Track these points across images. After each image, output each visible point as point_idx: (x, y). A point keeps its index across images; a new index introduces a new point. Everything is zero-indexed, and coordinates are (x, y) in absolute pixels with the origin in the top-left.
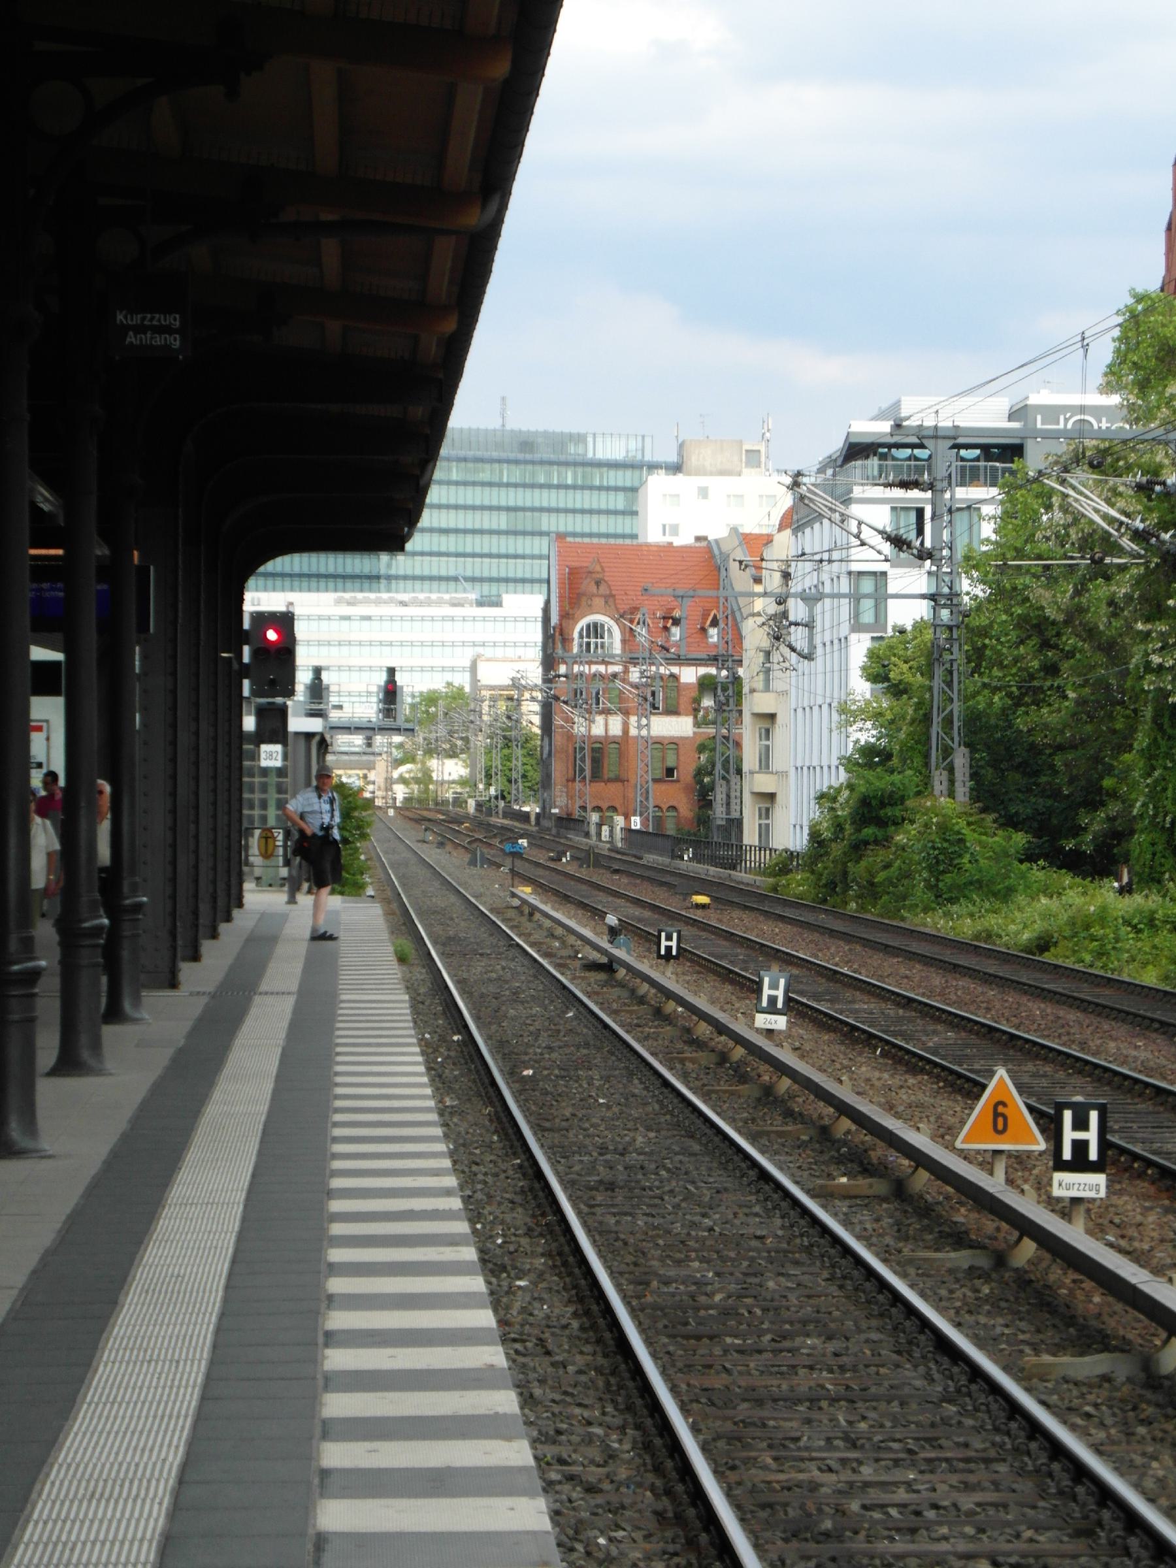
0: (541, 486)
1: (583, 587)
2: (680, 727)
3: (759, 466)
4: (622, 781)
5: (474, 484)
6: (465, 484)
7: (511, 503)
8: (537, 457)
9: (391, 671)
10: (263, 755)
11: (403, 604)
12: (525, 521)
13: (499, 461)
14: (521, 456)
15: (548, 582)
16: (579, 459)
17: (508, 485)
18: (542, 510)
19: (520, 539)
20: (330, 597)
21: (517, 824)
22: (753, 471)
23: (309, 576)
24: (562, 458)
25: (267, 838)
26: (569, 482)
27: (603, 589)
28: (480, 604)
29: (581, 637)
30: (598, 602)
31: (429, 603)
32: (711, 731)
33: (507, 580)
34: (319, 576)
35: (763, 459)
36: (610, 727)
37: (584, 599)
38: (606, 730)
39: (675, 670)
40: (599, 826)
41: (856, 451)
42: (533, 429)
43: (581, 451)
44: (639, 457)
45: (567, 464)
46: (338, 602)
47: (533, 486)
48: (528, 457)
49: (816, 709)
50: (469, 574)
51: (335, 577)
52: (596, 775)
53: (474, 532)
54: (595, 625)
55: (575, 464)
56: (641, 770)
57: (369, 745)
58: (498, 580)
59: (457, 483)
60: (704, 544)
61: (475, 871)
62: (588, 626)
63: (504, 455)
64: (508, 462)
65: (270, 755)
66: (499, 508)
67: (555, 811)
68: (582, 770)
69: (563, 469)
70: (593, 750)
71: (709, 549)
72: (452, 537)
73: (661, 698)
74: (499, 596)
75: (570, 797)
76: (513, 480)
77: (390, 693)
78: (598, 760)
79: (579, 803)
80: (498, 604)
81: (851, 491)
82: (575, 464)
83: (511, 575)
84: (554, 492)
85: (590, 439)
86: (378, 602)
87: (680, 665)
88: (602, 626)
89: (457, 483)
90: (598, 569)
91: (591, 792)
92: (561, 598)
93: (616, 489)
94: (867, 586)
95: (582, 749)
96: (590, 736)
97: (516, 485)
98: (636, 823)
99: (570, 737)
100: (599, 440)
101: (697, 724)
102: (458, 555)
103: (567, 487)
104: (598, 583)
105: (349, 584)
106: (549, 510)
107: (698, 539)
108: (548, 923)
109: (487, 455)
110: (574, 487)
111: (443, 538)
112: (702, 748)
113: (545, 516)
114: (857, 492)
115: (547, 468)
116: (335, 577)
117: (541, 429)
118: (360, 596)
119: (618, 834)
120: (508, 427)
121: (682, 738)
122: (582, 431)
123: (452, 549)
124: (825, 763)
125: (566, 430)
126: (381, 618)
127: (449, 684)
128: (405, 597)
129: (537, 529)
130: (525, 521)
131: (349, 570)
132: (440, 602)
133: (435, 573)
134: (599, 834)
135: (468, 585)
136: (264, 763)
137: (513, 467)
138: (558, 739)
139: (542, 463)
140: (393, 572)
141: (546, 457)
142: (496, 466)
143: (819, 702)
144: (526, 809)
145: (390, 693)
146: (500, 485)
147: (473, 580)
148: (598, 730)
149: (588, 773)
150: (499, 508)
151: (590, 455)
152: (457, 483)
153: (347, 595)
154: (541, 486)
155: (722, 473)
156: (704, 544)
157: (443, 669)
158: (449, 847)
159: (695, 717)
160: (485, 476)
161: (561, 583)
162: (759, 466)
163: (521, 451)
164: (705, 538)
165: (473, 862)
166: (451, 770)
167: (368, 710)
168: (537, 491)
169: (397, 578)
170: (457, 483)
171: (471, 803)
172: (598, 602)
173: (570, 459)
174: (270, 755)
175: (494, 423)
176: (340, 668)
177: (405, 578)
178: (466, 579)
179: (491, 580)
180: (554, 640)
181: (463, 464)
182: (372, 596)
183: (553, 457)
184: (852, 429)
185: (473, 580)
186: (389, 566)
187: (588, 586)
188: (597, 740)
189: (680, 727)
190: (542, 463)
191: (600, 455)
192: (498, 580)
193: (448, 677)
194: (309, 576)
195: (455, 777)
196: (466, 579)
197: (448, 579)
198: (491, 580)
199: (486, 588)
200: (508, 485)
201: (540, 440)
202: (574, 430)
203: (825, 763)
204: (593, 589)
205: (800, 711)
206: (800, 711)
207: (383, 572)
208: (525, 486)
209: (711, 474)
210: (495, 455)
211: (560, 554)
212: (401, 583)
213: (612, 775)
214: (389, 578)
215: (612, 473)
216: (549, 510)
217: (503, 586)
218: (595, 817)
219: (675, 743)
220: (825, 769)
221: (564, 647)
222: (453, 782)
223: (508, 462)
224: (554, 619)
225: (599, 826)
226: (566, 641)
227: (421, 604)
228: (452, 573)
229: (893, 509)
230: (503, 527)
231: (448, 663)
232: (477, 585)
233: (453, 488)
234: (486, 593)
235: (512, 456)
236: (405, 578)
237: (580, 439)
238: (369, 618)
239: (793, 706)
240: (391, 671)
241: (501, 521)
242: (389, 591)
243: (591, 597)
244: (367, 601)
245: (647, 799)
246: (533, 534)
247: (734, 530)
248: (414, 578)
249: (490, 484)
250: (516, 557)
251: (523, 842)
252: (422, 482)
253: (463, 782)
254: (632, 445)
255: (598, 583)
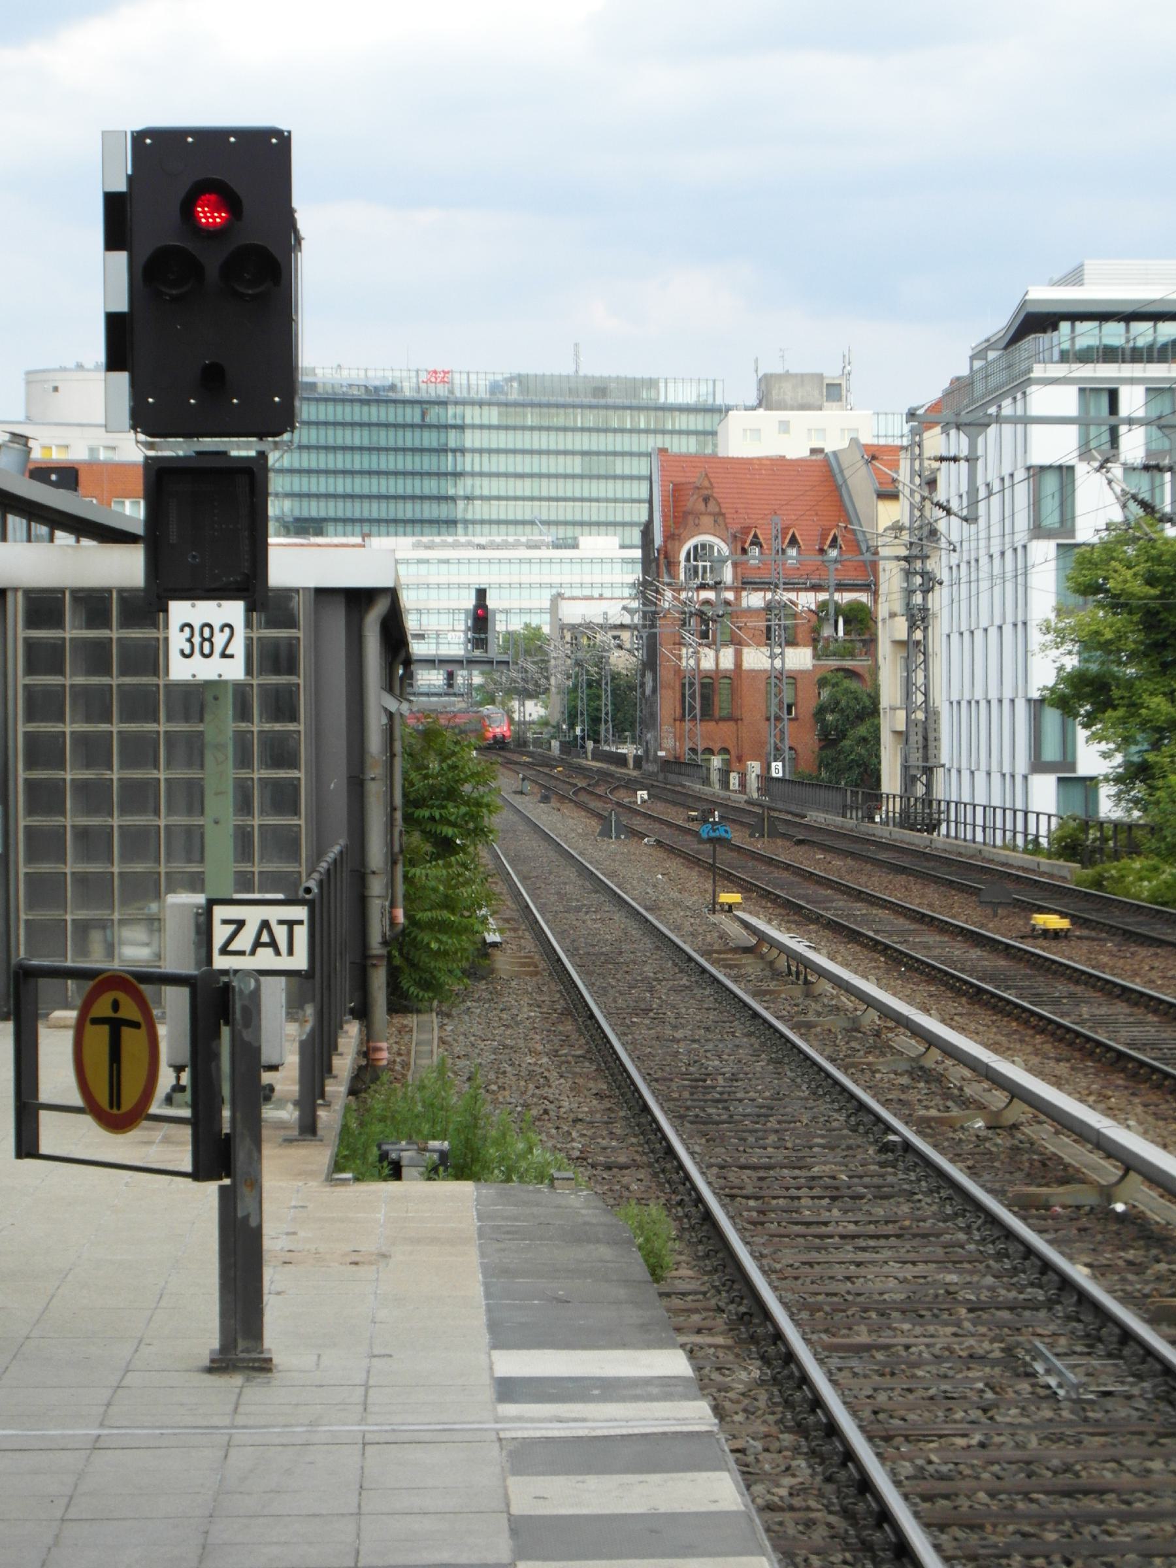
0: (615, 431)
1: (690, 504)
2: (800, 658)
3: (840, 400)
4: (736, 720)
5: (549, 429)
6: (540, 428)
7: (586, 448)
8: (610, 401)
9: (481, 594)
10: (177, 641)
11: (481, 547)
12: (599, 465)
13: (574, 406)
14: (594, 401)
15: (650, 502)
16: (652, 404)
17: (583, 430)
18: (615, 454)
19: (594, 483)
20: (409, 540)
21: (613, 768)
22: (835, 404)
23: (387, 521)
24: (635, 402)
25: (116, 1026)
26: (642, 426)
27: (712, 506)
28: (556, 546)
29: (688, 559)
30: (707, 521)
31: (504, 546)
32: (833, 663)
33: (582, 524)
34: (396, 521)
35: (844, 393)
36: (721, 660)
37: (691, 518)
38: (717, 665)
39: (792, 596)
40: (725, 773)
41: (1036, 322)
42: (606, 374)
43: (653, 394)
44: (710, 401)
45: (640, 408)
46: (416, 546)
47: (606, 430)
48: (602, 402)
49: (979, 634)
50: (544, 517)
51: (413, 522)
52: (707, 713)
53: (558, 453)
54: (703, 546)
55: (647, 408)
56: (754, 705)
57: (450, 685)
58: (574, 524)
59: (532, 428)
60: (820, 457)
61: (613, 845)
62: (696, 547)
63: (577, 401)
64: (582, 407)
65: (202, 641)
66: (573, 453)
67: (661, 754)
68: (692, 708)
69: (635, 413)
70: (703, 685)
71: (826, 462)
72: (528, 482)
73: (778, 629)
74: (575, 539)
75: (680, 738)
76: (587, 425)
77: (481, 619)
78: (707, 697)
79: (689, 744)
80: (575, 546)
81: (1030, 370)
82: (647, 408)
83: (586, 518)
84: (627, 436)
85: (662, 385)
86: (456, 545)
87: (798, 590)
88: (711, 547)
89: (532, 428)
90: (706, 483)
91: (702, 733)
92: (665, 516)
93: (688, 433)
94: (1051, 483)
95: (692, 684)
96: (700, 671)
97: (589, 430)
98: (777, 769)
99: (678, 670)
100: (671, 385)
101: (816, 656)
102: (532, 499)
103: (639, 431)
104: (706, 500)
105: (426, 529)
106: (623, 454)
107: (813, 451)
108: (915, 1047)
109: (561, 400)
110: (647, 431)
111: (519, 482)
112: (822, 683)
113: (619, 460)
114: (1038, 371)
115: (620, 412)
116: (413, 522)
117: (614, 375)
118: (437, 539)
119: (753, 782)
120: (581, 373)
121: (801, 672)
122: (654, 376)
123: (528, 493)
124: (993, 695)
125: (638, 375)
126: (459, 562)
127: (527, 626)
128: (482, 540)
129: (611, 473)
130: (599, 465)
131: (426, 515)
132: (516, 545)
133: (511, 517)
134: (725, 784)
135: (544, 528)
136: (182, 669)
137: (587, 412)
138: (665, 674)
139: (616, 408)
140: (469, 516)
141: (619, 401)
142: (571, 410)
143: (984, 623)
144: (623, 750)
145: (481, 619)
146: (574, 430)
147: (548, 523)
148: (707, 664)
149: (698, 711)
150: (573, 453)
151: (662, 400)
152: (532, 428)
153: (425, 539)
154: (615, 431)
155: (803, 407)
156: (820, 457)
157: (521, 611)
158: (554, 802)
159: (815, 649)
160: (560, 421)
161: (664, 501)
162: (840, 400)
163: (594, 396)
164: (821, 451)
165: (606, 833)
166: (533, 710)
167: (455, 644)
168: (610, 436)
169: (474, 522)
170: (532, 428)
171: (555, 744)
172: (707, 521)
173: (643, 403)
174: (202, 641)
175: (567, 369)
176: (418, 587)
177: (482, 522)
178: (543, 523)
179: (566, 523)
180: (656, 562)
181: (536, 410)
182: (450, 539)
183: (627, 402)
184: (1030, 297)
185: (548, 523)
186: (466, 510)
187: (693, 502)
188: (707, 675)
189: (800, 658)
190: (616, 408)
191: (671, 400)
192: (574, 524)
193: (526, 618)
194: (387, 521)
195: (535, 717)
196: (543, 523)
197: (524, 523)
198: (566, 523)
199: (561, 532)
200: (583, 430)
201: (613, 385)
202: (646, 376)
203: (993, 695)
204: (701, 506)
205: (955, 637)
206: (955, 637)
207: (460, 516)
208: (598, 430)
209: (792, 409)
210: (569, 400)
211: (663, 469)
212: (478, 527)
213: (724, 713)
214: (466, 522)
215: (684, 417)
216: (623, 454)
217: (578, 529)
218: (716, 762)
219: (794, 678)
220: (994, 704)
221: (669, 571)
222: (533, 723)
223: (582, 407)
224: (658, 540)
225: (725, 773)
226: (671, 565)
227: (498, 547)
228: (528, 517)
229: (1082, 390)
230: (578, 471)
231: (526, 604)
232: (553, 529)
233: (527, 433)
234: (561, 535)
235: (586, 401)
236: (482, 522)
237: (652, 383)
238: (447, 562)
239: (946, 631)
240: (481, 594)
241: (575, 465)
242: (466, 534)
243: (698, 515)
244: (444, 545)
245: (782, 740)
246: (606, 477)
247: (855, 441)
248: (490, 522)
249: (565, 429)
250: (590, 500)
251: (643, 794)
252: (253, 1223)
253: (545, 723)
254: (703, 389)
255: (706, 500)
